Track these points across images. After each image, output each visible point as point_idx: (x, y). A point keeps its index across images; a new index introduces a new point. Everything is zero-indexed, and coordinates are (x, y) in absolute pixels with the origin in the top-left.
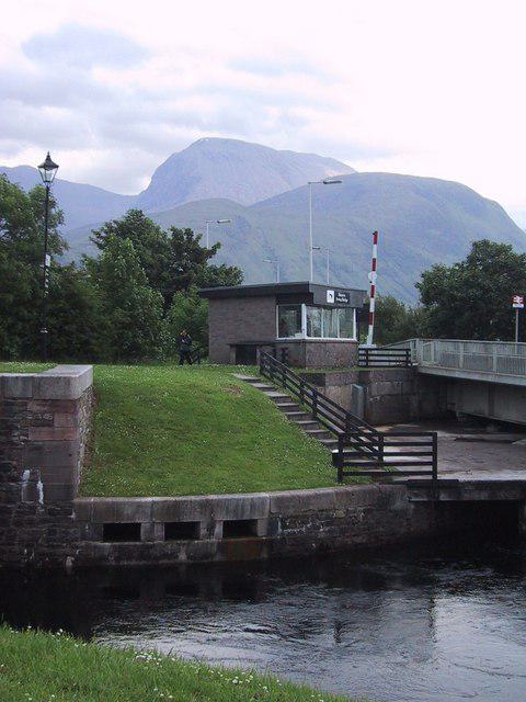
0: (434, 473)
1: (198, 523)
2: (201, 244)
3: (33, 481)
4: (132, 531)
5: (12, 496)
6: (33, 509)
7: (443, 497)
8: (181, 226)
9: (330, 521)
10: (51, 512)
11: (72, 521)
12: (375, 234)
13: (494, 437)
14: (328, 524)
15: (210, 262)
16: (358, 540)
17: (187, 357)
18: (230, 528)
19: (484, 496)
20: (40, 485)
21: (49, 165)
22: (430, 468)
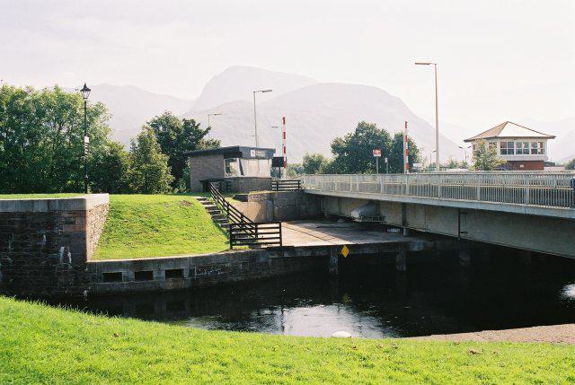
0: (281, 243)
1: (183, 270)
2: (200, 128)
3: (66, 253)
4: (118, 277)
5: (56, 261)
6: (66, 266)
7: (286, 255)
8: (188, 119)
9: (224, 269)
10: (76, 268)
11: (86, 272)
12: (284, 118)
13: (341, 225)
14: (222, 270)
15: (206, 138)
16: (240, 278)
17: (146, 190)
18: (169, 274)
19: (308, 254)
20: (69, 254)
21: (86, 89)
22: (278, 240)
